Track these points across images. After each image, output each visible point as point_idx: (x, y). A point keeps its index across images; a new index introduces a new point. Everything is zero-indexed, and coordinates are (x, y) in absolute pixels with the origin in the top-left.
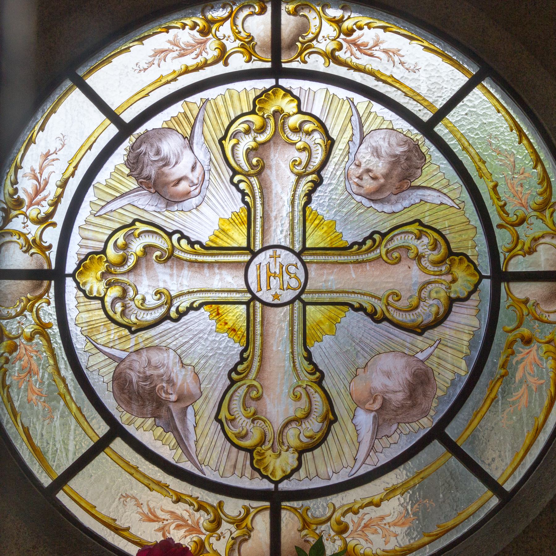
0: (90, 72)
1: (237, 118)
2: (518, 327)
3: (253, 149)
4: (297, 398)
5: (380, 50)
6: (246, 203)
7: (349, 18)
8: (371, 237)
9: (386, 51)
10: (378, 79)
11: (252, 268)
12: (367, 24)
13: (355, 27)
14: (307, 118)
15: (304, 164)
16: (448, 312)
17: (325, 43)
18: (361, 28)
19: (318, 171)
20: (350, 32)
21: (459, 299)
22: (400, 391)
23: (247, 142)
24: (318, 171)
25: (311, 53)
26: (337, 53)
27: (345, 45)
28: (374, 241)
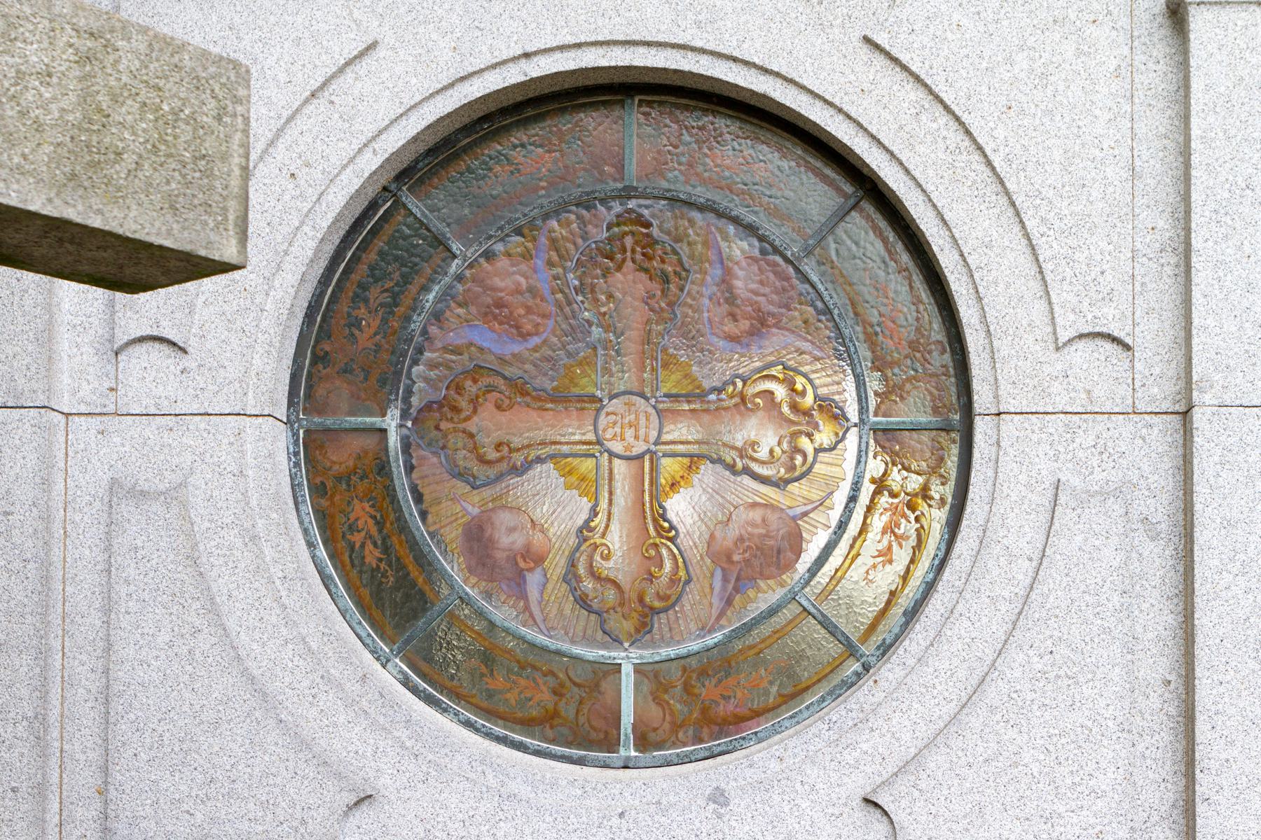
0: (868, 218)
1: (810, 381)
2: (575, 684)
3: (773, 400)
4: (498, 446)
5: (890, 542)
6: (661, 506)
7: (930, 506)
8: (672, 527)
9: (890, 548)
10: (855, 540)
11: (652, 438)
12: (922, 527)
13: (918, 513)
14: (810, 459)
15: (755, 455)
16: (590, 610)
17: (898, 478)
18: (917, 519)
19: (747, 471)
20: (912, 507)
21: (603, 622)
22: (996, 397)
23: (780, 392)
24: (747, 471)
25: (887, 464)
26: (886, 493)
27: (896, 501)
28: (669, 531)
